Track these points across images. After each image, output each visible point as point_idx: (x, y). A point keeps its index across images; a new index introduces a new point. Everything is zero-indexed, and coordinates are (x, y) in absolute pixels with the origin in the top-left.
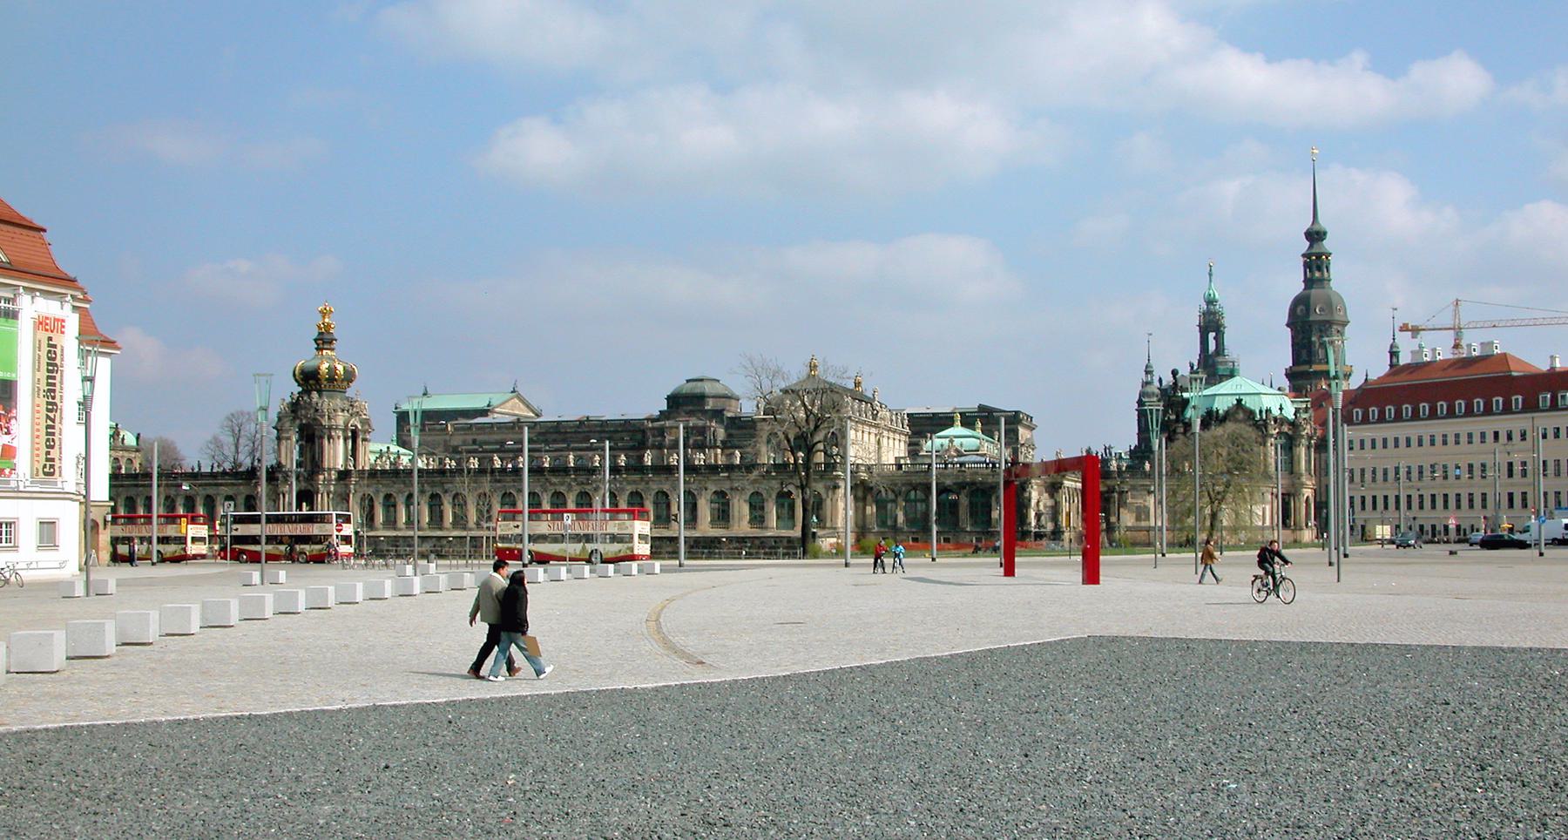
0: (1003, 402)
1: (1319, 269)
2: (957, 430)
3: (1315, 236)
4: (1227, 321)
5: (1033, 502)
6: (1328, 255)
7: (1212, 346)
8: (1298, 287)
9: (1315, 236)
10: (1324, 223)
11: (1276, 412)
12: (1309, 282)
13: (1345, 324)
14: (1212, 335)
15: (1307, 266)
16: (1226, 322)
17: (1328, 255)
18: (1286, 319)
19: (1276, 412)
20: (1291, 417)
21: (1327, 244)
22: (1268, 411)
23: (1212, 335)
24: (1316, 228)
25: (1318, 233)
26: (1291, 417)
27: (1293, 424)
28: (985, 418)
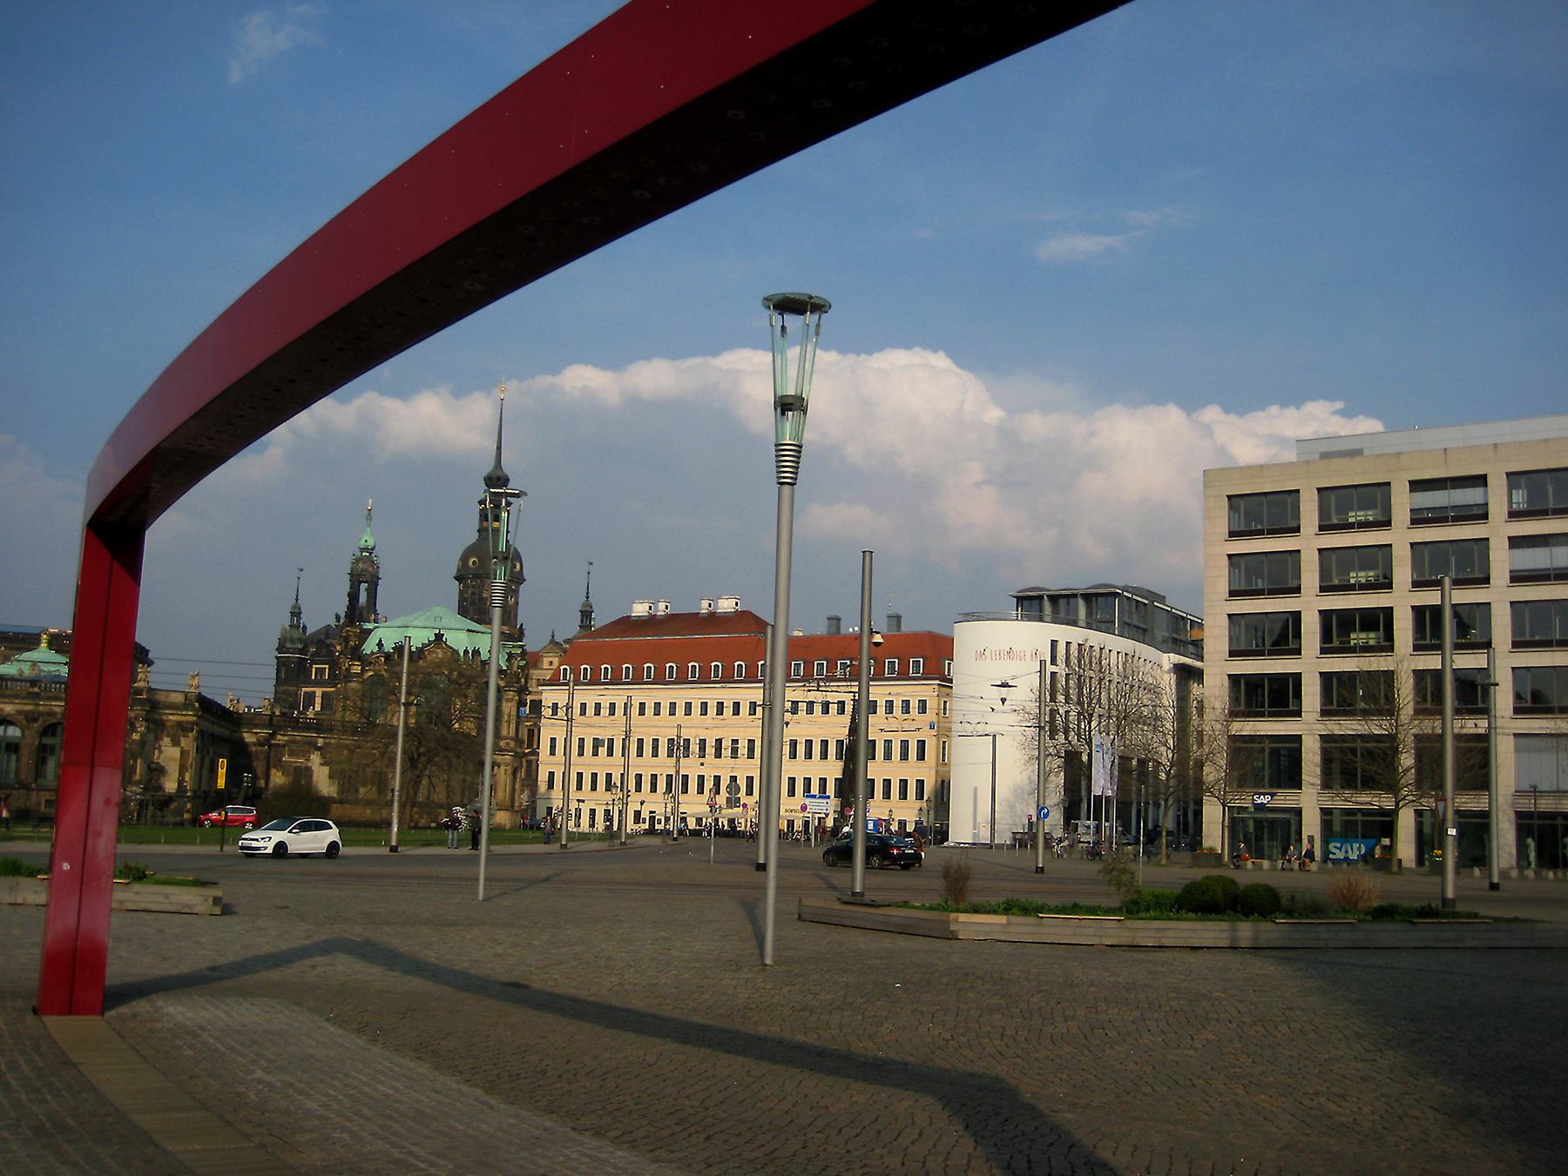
10: (508, 467)
14: (364, 586)
22: (476, 652)
23: (364, 586)
24: (499, 473)
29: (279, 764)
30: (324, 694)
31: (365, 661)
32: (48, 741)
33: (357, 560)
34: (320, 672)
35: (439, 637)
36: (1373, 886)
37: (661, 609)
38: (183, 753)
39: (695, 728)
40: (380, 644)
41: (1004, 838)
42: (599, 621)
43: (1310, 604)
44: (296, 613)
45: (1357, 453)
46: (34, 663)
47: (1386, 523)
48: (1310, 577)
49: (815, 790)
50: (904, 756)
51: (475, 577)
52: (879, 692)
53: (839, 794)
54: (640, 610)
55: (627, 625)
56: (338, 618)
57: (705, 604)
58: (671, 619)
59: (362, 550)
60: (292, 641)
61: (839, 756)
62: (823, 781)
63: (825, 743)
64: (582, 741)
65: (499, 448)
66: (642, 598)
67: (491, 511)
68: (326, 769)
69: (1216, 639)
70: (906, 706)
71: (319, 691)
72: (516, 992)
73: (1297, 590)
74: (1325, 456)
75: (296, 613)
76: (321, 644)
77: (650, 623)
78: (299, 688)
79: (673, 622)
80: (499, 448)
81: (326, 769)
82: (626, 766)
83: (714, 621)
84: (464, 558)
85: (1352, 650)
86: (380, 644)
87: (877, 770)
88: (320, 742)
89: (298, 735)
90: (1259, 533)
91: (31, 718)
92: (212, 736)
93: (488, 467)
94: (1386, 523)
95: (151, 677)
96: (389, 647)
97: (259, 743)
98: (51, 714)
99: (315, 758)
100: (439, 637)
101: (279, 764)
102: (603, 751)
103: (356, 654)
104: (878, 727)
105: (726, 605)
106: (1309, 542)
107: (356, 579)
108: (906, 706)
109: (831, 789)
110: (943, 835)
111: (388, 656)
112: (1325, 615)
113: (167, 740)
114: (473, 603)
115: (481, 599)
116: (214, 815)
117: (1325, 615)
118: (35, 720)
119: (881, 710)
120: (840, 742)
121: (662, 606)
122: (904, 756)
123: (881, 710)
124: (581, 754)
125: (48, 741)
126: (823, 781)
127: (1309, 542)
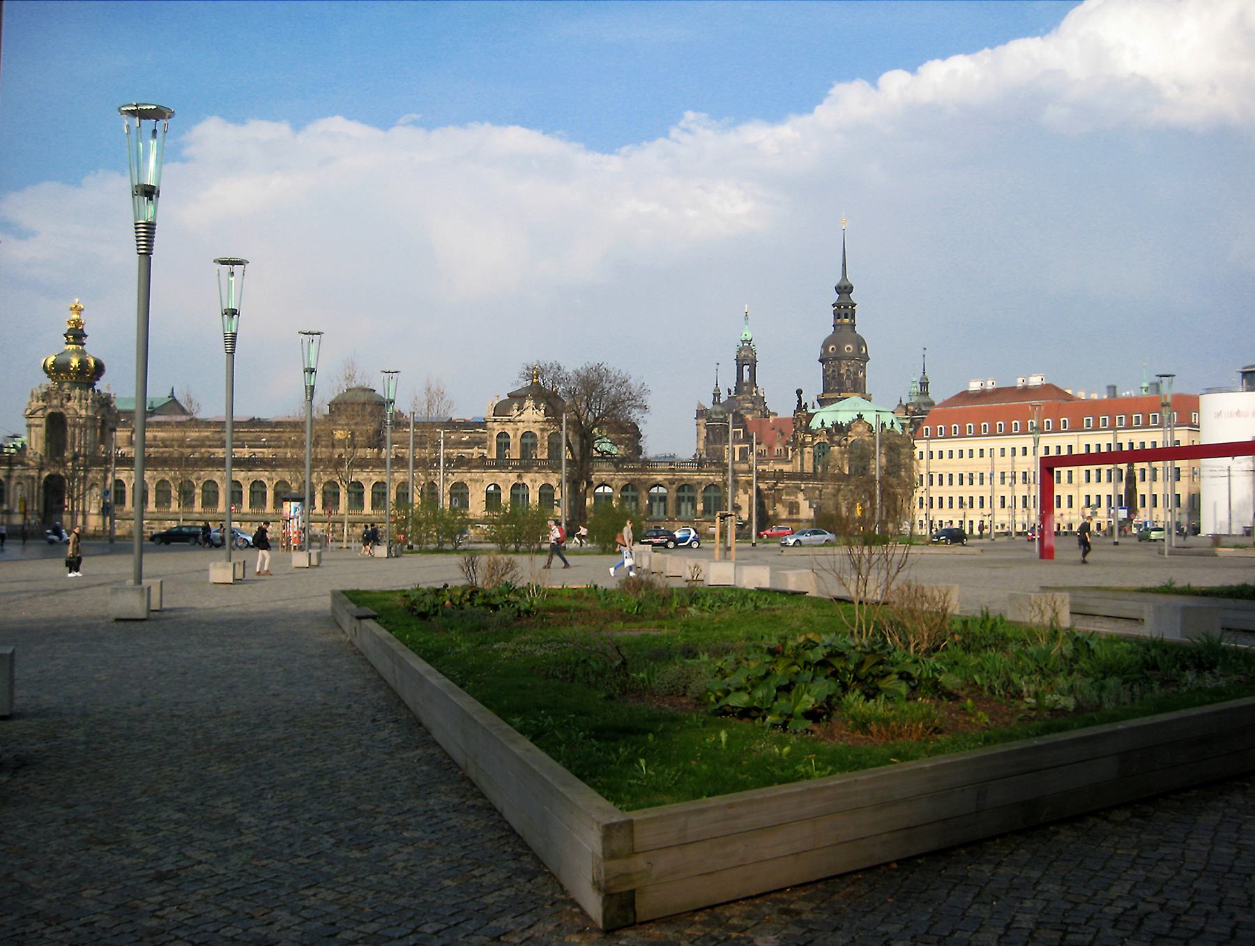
10: (851, 279)
11: (888, 426)
22: (884, 425)
23: (746, 368)
29: (780, 501)
30: (741, 449)
31: (814, 434)
32: (681, 494)
33: (739, 352)
35: (860, 416)
37: (989, 386)
38: (750, 498)
40: (823, 423)
41: (1237, 529)
51: (835, 359)
54: (975, 386)
55: (966, 396)
57: (1020, 380)
58: (997, 391)
59: (743, 342)
60: (716, 413)
65: (844, 265)
66: (975, 378)
67: (844, 309)
72: (1098, 588)
77: (982, 395)
79: (998, 393)
80: (844, 265)
82: (993, 491)
83: (1026, 391)
84: (825, 346)
86: (823, 423)
88: (803, 487)
89: (791, 483)
91: (672, 482)
93: (837, 279)
96: (828, 425)
97: (770, 489)
98: (682, 480)
99: (801, 496)
100: (860, 416)
101: (780, 501)
103: (808, 430)
105: (1035, 381)
110: (1196, 530)
111: (828, 430)
113: (741, 491)
114: (834, 378)
115: (839, 374)
116: (768, 532)
121: (990, 383)
125: (681, 494)
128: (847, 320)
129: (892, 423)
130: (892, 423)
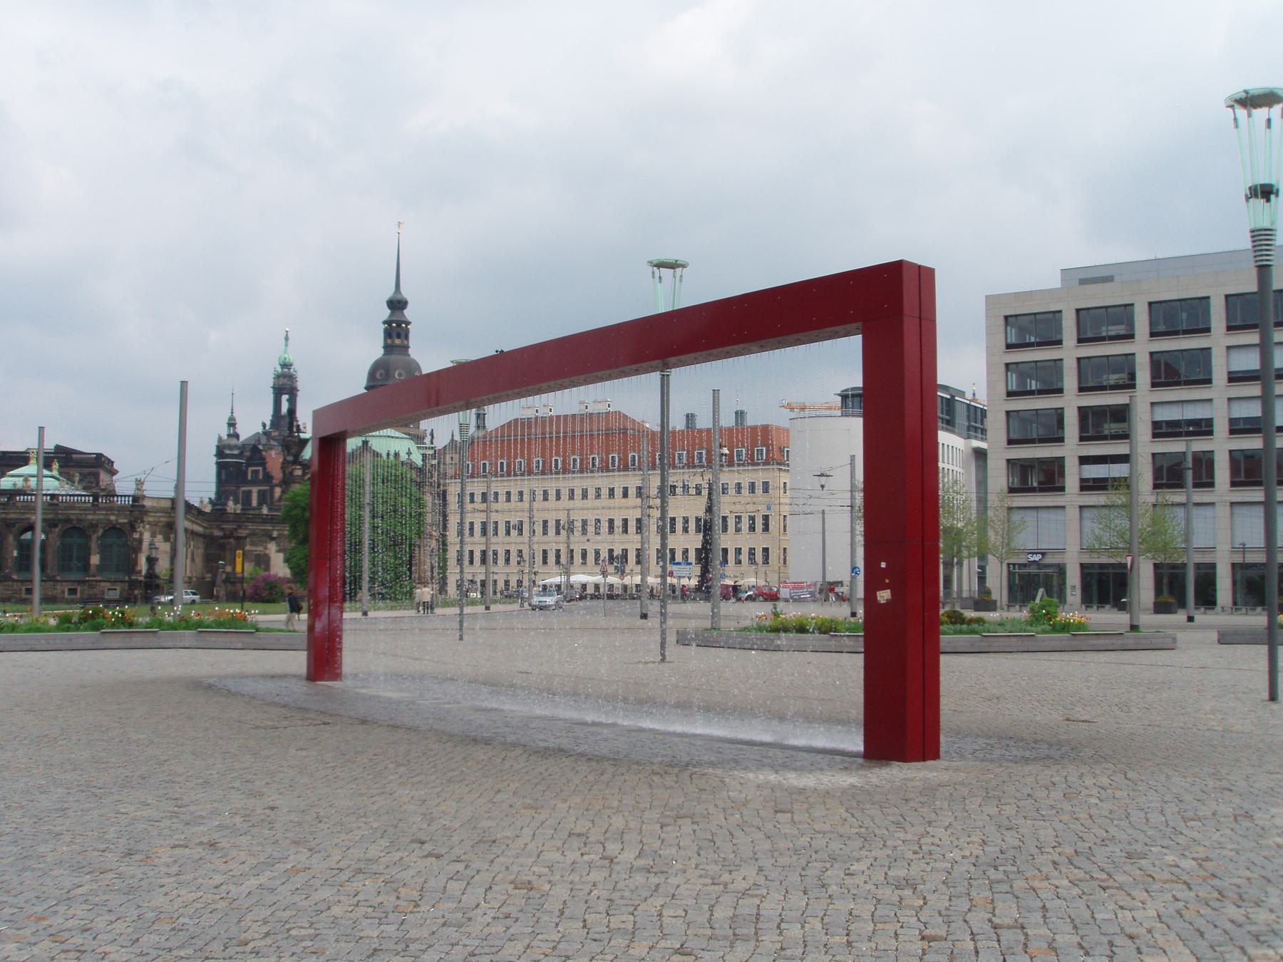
0: (85, 445)
1: (399, 336)
2: (31, 469)
3: (397, 305)
4: (301, 384)
5: (145, 545)
6: (408, 323)
7: (285, 408)
8: (378, 352)
9: (397, 305)
10: (406, 293)
11: (403, 457)
12: (388, 348)
13: (1246, 92)
14: (285, 397)
15: (388, 334)
16: (300, 385)
17: (408, 323)
18: (299, 394)
19: (403, 457)
20: (419, 463)
21: (408, 313)
22: (397, 455)
23: (285, 397)
24: (399, 297)
25: (399, 302)
26: (419, 463)
27: (420, 471)
28: (65, 459)
30: (259, 491)
33: (278, 377)
34: (256, 472)
36: (715, 445)
39: (583, 510)
42: (750, 421)
43: (1071, 402)
44: (232, 424)
45: (1108, 279)
46: (26, 478)
47: (1130, 336)
48: (1070, 381)
49: (679, 558)
50: (752, 528)
52: (729, 477)
53: (699, 560)
56: (264, 425)
60: (230, 447)
61: (698, 530)
62: (686, 552)
63: (686, 520)
64: (472, 524)
68: (281, 555)
69: (996, 426)
70: (752, 487)
71: (255, 490)
73: (1060, 391)
74: (1083, 282)
75: (232, 424)
76: (254, 452)
78: (238, 488)
81: (281, 555)
85: (1104, 438)
87: (726, 541)
88: (275, 534)
90: (1031, 441)
92: (192, 532)
93: (389, 292)
94: (1130, 336)
95: (112, 484)
99: (272, 547)
102: (514, 533)
104: (727, 506)
106: (1069, 352)
107: (278, 391)
108: (752, 487)
109: (692, 556)
112: (1081, 409)
113: (160, 537)
117: (1081, 409)
118: (56, 526)
119: (732, 491)
120: (698, 520)
122: (752, 528)
123: (732, 491)
124: (472, 534)
126: (686, 552)
127: (1069, 352)
128: (398, 342)
129: (409, 453)
130: (409, 453)
